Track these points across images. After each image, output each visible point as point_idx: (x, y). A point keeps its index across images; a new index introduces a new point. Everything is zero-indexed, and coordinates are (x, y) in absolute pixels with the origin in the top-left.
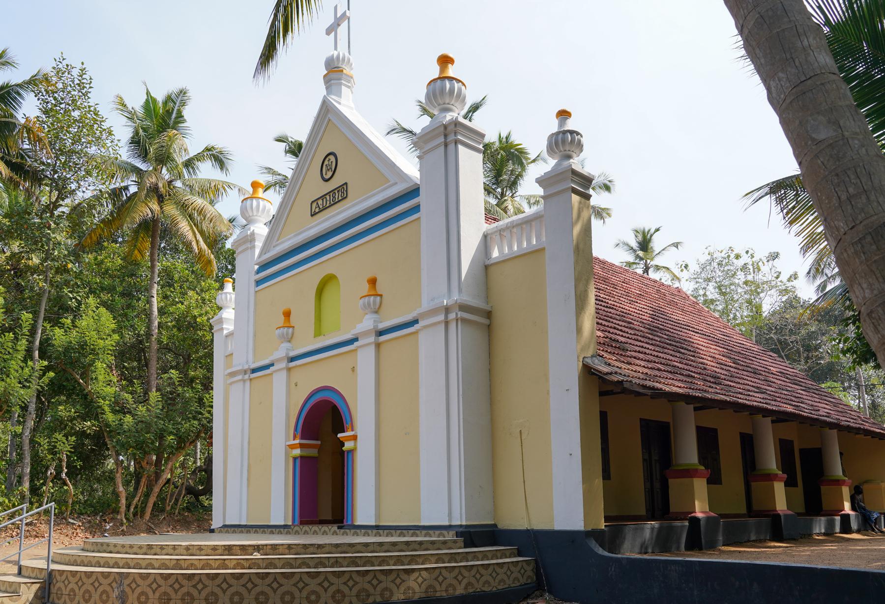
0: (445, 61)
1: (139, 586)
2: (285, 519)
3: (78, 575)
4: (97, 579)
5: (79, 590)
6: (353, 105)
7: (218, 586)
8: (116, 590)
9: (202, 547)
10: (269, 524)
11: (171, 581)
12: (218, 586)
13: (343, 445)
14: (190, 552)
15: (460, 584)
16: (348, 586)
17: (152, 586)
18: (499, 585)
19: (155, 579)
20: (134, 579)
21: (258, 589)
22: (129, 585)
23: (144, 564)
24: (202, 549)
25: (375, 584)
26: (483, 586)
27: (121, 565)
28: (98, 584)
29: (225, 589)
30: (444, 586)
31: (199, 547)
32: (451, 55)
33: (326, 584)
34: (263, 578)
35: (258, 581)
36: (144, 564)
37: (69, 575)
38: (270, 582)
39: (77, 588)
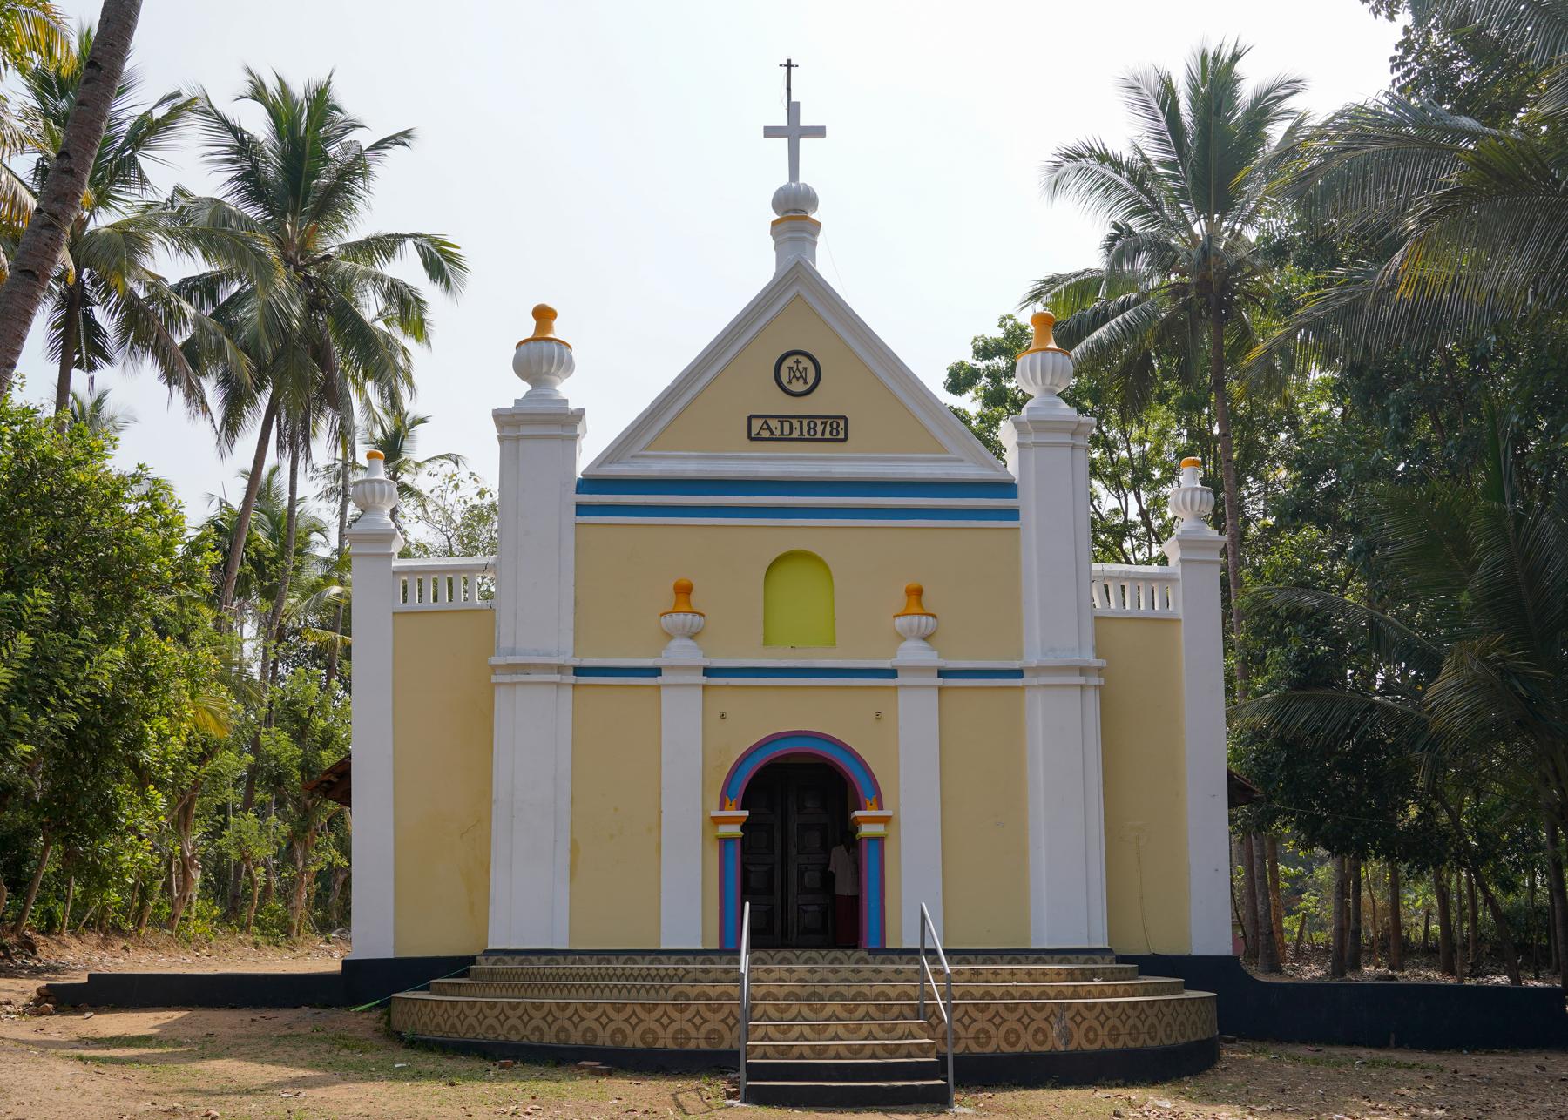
0: (544, 315)
1: (611, 1020)
2: (704, 941)
3: (1140, 1007)
6: (71, 397)
7: (689, 1021)
8: (1056, 1026)
11: (1118, 1011)
12: (689, 1021)
14: (1033, 977)
18: (532, 1033)
20: (1078, 1010)
21: (676, 1026)
25: (576, 1022)
30: (671, 1030)
32: (551, 305)
34: (682, 1011)
37: (465, 1007)
39: (546, 1025)
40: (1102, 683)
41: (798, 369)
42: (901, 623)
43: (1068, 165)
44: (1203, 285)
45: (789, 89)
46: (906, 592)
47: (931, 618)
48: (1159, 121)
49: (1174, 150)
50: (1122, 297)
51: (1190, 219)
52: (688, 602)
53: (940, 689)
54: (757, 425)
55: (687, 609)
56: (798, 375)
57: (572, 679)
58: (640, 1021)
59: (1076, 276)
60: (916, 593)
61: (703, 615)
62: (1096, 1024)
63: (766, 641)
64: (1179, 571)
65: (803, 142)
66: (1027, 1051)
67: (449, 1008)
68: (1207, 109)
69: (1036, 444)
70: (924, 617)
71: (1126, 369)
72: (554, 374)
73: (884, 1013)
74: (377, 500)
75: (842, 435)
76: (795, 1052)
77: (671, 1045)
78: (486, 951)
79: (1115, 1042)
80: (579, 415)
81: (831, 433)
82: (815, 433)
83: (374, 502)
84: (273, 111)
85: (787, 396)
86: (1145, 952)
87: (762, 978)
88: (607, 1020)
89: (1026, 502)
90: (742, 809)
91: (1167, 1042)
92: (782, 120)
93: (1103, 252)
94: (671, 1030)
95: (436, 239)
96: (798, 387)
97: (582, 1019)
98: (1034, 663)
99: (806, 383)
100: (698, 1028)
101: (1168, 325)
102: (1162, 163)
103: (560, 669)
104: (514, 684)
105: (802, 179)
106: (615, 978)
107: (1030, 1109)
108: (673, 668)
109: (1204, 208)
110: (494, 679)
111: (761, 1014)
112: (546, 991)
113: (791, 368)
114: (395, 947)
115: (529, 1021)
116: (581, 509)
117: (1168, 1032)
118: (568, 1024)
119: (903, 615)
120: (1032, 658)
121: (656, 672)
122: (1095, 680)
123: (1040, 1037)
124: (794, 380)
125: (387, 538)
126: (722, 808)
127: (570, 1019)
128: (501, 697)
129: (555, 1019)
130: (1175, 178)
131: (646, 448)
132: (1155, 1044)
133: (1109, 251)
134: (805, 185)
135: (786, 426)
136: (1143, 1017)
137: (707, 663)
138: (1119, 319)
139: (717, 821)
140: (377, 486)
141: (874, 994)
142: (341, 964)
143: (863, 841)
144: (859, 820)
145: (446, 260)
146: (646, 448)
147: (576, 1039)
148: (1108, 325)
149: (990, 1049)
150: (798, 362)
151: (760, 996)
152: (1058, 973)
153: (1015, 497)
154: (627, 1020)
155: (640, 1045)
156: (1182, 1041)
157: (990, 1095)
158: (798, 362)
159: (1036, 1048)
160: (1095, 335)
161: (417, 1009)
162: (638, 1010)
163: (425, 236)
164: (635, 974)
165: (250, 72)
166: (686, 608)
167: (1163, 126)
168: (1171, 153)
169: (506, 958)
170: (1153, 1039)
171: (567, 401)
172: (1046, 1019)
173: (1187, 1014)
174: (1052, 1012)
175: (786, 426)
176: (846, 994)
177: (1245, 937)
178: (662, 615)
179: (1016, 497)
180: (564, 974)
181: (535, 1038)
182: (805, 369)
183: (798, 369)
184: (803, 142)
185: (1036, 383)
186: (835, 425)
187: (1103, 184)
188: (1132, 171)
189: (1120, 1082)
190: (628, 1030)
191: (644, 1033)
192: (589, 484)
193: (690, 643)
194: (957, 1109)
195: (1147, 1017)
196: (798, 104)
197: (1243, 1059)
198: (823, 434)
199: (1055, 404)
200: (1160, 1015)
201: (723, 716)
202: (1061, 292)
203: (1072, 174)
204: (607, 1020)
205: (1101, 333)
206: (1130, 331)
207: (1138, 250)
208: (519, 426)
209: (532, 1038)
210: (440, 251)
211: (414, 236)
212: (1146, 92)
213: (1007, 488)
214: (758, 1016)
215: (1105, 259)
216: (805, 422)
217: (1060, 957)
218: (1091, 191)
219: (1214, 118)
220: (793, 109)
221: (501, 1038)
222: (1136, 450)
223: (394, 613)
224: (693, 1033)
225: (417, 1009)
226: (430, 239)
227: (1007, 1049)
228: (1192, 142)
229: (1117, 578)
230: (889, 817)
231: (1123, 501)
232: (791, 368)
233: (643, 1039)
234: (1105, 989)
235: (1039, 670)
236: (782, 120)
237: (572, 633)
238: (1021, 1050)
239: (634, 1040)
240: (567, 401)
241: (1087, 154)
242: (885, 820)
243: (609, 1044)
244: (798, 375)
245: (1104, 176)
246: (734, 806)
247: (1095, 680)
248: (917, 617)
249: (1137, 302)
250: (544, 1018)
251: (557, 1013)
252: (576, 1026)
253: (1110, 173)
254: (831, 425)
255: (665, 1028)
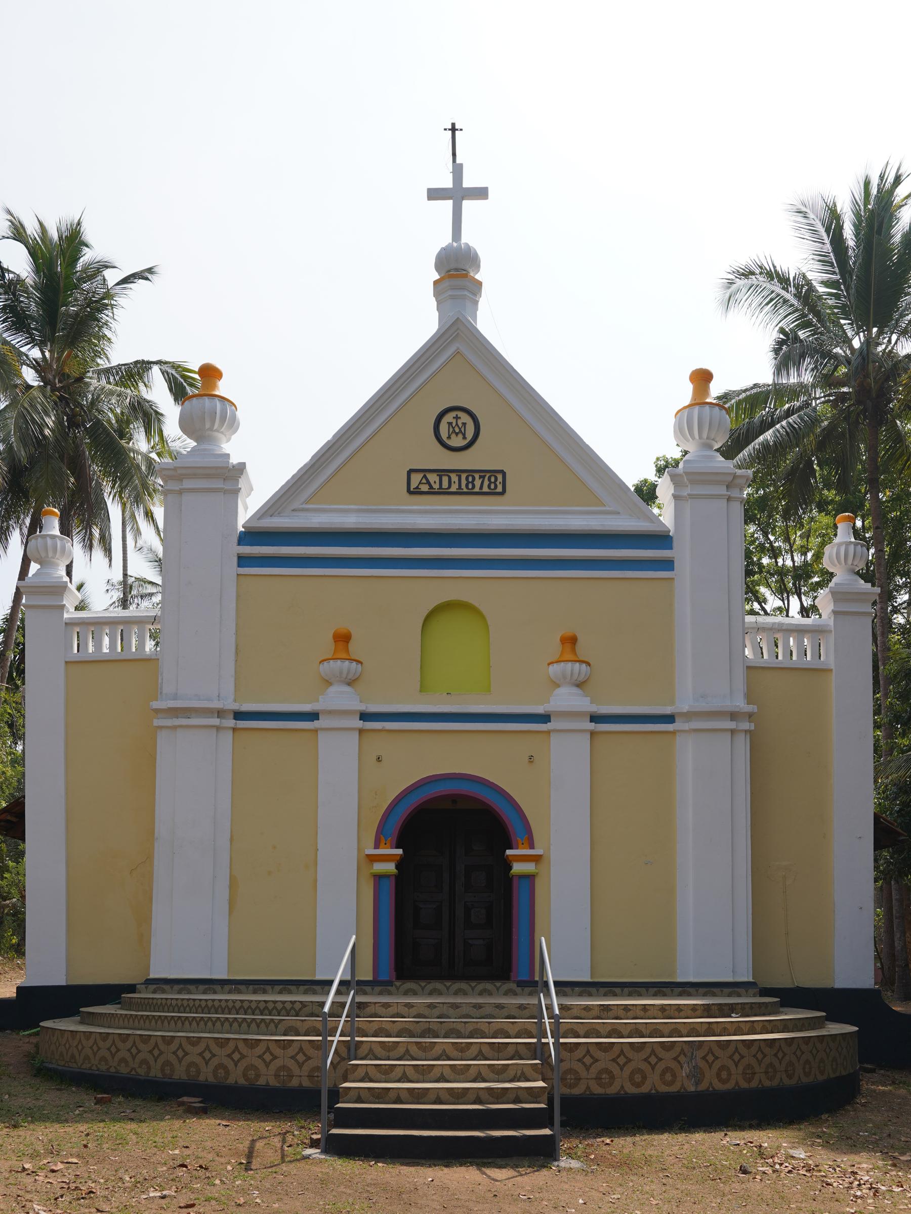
3: (777, 1044)
4: (208, 1047)
5: (780, 1063)
8: (685, 1066)
9: (681, 1007)
10: (314, 979)
11: (754, 1049)
13: (510, 868)
14: (666, 1013)
15: (710, 1067)
16: (618, 1064)
17: (625, 1060)
18: (140, 1067)
19: (736, 1048)
21: (278, 1063)
22: (704, 1058)
23: (666, 1031)
24: (682, 1010)
26: (118, 1065)
27: (770, 1029)
28: (178, 1053)
29: (301, 1062)
30: (273, 1067)
31: (677, 1007)
32: (219, 366)
33: (653, 1060)
34: (284, 1048)
35: (278, 1051)
36: (666, 1031)
38: (294, 1053)
40: (753, 728)
41: (457, 424)
42: (555, 670)
43: (740, 283)
44: (862, 393)
45: (454, 154)
46: (561, 640)
47: (584, 665)
48: (823, 244)
49: (837, 270)
50: (787, 406)
51: (850, 333)
52: (347, 651)
53: (593, 734)
54: (416, 479)
55: (344, 656)
56: (457, 430)
57: (231, 723)
58: (243, 1057)
59: (745, 391)
60: (570, 641)
61: (361, 663)
62: (730, 1064)
63: (423, 688)
64: (831, 622)
65: (466, 204)
66: (653, 1091)
67: (82, 1038)
68: (870, 225)
69: (692, 496)
70: (578, 664)
71: (791, 475)
72: (217, 431)
73: (498, 1052)
74: (50, 554)
75: (500, 489)
76: (392, 1095)
77: (273, 1082)
78: (147, 980)
79: (749, 1081)
80: (241, 468)
81: (489, 487)
82: (474, 486)
83: (47, 556)
84: (33, 252)
85: (439, 445)
86: (788, 984)
87: (380, 1013)
88: (210, 1055)
89: (681, 553)
90: (397, 847)
91: (805, 1080)
92: (447, 182)
93: (771, 355)
94: (273, 1067)
95: (179, 366)
96: (457, 442)
97: (186, 1054)
98: (685, 708)
99: (464, 438)
100: (300, 1065)
101: (829, 432)
102: (825, 283)
103: (220, 713)
104: (175, 728)
105: (464, 239)
106: (242, 1011)
107: (648, 1161)
108: (330, 712)
109: (862, 323)
110: (156, 722)
111: (366, 1052)
112: (163, 1023)
113: (450, 424)
114: (67, 975)
115: (137, 1054)
116: (243, 561)
117: (807, 1070)
118: (173, 1059)
119: (557, 662)
120: (682, 706)
121: (313, 716)
122: (746, 725)
123: (668, 1077)
124: (453, 436)
125: (60, 589)
126: (377, 846)
127: (174, 1053)
128: (162, 739)
129: (161, 1053)
130: (838, 297)
131: (307, 502)
132: (793, 1082)
133: (776, 354)
134: (467, 244)
135: (445, 480)
136: (780, 1055)
137: (362, 707)
138: (784, 423)
139: (372, 859)
140: (49, 541)
141: (492, 1032)
142: (15, 991)
143: (514, 877)
144: (510, 858)
145: (188, 384)
146: (307, 502)
147: (180, 1073)
148: (774, 428)
149: (613, 1090)
150: (457, 418)
151: (372, 1032)
152: (694, 1008)
153: (670, 547)
154: (229, 1056)
155: (242, 1081)
156: (821, 1078)
157: (608, 1141)
158: (457, 418)
159: (663, 1089)
160: (761, 438)
161: (55, 1038)
162: (241, 1045)
163: (169, 363)
164: (253, 1007)
165: (9, 212)
166: (344, 656)
167: (828, 247)
168: (834, 273)
169: (165, 987)
170: (790, 1077)
171: (228, 455)
172: (675, 1059)
173: (828, 1050)
174: (682, 1052)
175: (445, 480)
176: (463, 1031)
177: (882, 968)
178: (320, 663)
179: (671, 548)
180: (188, 1005)
181: (142, 1071)
182: (464, 424)
183: (457, 424)
184: (466, 204)
185: (693, 438)
186: (493, 479)
187: (772, 300)
188: (797, 287)
189: (754, 1122)
190: (231, 1065)
191: (247, 1069)
192: (251, 536)
193: (347, 689)
194: (564, 1162)
195: (785, 1054)
196: (461, 165)
197: (884, 1092)
198: (481, 488)
199: (712, 457)
200: (799, 1053)
201: (379, 759)
202: (733, 406)
203: (744, 290)
204: (210, 1055)
205: (768, 435)
206: (794, 436)
207: (802, 356)
208: (181, 480)
209: (139, 1071)
210: (184, 377)
211: (159, 362)
212: (811, 216)
213: (662, 539)
214: (364, 1055)
215: (774, 362)
216: (464, 476)
217: (705, 990)
218: (761, 306)
219: (876, 236)
220: (458, 171)
221: (113, 1070)
222: (798, 559)
223: (66, 662)
224: (296, 1070)
225: (55, 1038)
226: (175, 366)
227: (631, 1090)
228: (854, 263)
229: (771, 629)
230: (541, 856)
231: (786, 602)
232: (450, 424)
233: (245, 1075)
234: (742, 1025)
235: (689, 716)
236: (447, 182)
237: (233, 679)
238: (647, 1091)
239: (236, 1077)
240: (228, 455)
241: (757, 271)
242: (537, 859)
243: (211, 1079)
244: (457, 430)
245: (773, 292)
246: (388, 844)
247: (746, 725)
248: (570, 664)
249: (800, 408)
250: (151, 1052)
251: (162, 1047)
252: (180, 1060)
253: (778, 289)
254: (489, 479)
255: (267, 1065)
